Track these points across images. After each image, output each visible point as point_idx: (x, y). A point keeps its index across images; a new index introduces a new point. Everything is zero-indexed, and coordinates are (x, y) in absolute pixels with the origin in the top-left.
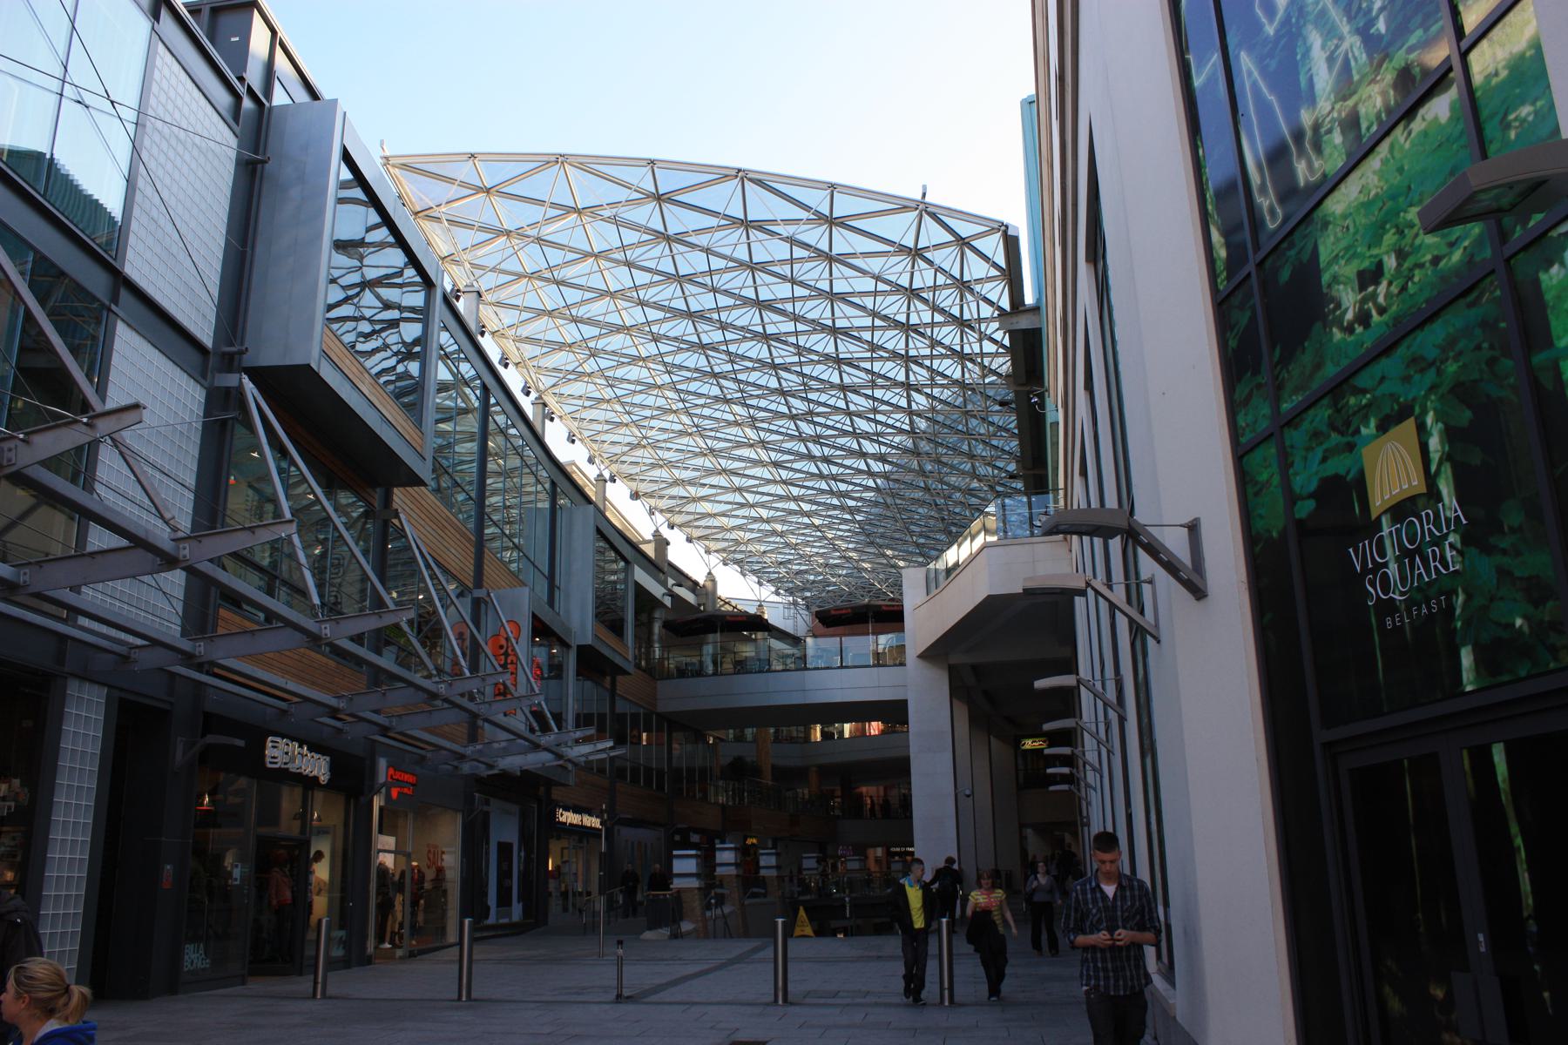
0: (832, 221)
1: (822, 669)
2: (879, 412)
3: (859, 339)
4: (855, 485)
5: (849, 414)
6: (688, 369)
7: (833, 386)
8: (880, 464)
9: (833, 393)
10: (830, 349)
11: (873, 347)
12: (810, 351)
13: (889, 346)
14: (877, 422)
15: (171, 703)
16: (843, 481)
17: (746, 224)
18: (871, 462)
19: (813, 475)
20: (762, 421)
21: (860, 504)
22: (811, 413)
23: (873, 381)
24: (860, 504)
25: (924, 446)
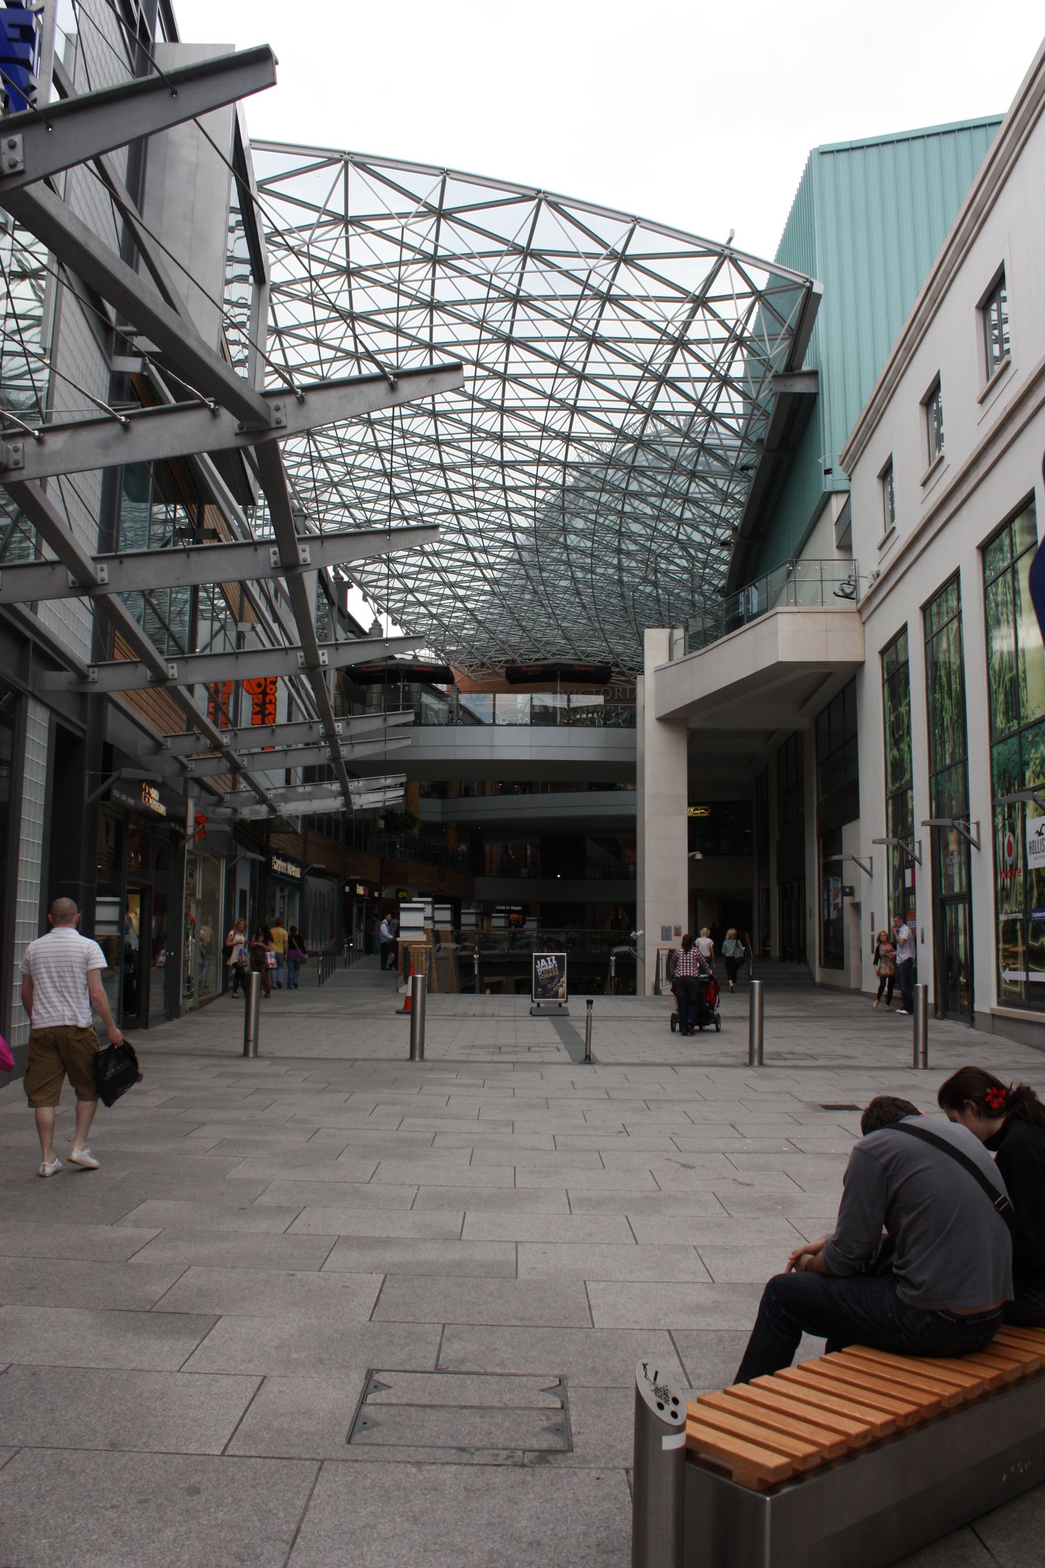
0: (441, 214)
1: (521, 725)
2: (478, 489)
3: (460, 422)
4: (465, 575)
5: (456, 513)
6: (298, 455)
7: (433, 466)
8: (484, 556)
9: (434, 472)
10: (431, 432)
11: (472, 428)
12: (414, 434)
13: (420, 431)
14: (475, 499)
15: (84, 732)
16: (453, 572)
17: (346, 221)
18: (476, 554)
19: (426, 568)
20: (369, 502)
21: (469, 593)
22: (415, 492)
23: (472, 460)
24: (469, 593)
25: (526, 556)
